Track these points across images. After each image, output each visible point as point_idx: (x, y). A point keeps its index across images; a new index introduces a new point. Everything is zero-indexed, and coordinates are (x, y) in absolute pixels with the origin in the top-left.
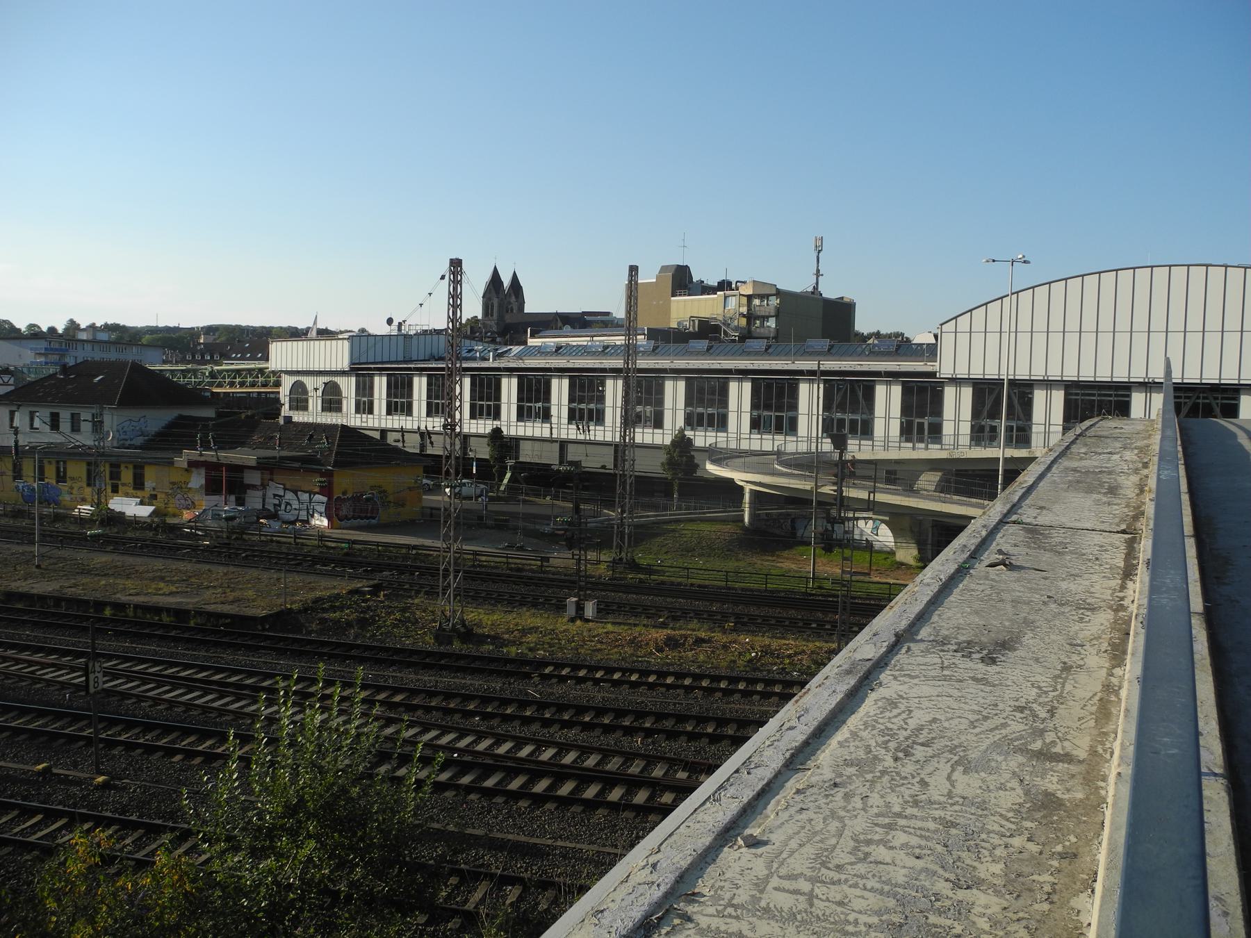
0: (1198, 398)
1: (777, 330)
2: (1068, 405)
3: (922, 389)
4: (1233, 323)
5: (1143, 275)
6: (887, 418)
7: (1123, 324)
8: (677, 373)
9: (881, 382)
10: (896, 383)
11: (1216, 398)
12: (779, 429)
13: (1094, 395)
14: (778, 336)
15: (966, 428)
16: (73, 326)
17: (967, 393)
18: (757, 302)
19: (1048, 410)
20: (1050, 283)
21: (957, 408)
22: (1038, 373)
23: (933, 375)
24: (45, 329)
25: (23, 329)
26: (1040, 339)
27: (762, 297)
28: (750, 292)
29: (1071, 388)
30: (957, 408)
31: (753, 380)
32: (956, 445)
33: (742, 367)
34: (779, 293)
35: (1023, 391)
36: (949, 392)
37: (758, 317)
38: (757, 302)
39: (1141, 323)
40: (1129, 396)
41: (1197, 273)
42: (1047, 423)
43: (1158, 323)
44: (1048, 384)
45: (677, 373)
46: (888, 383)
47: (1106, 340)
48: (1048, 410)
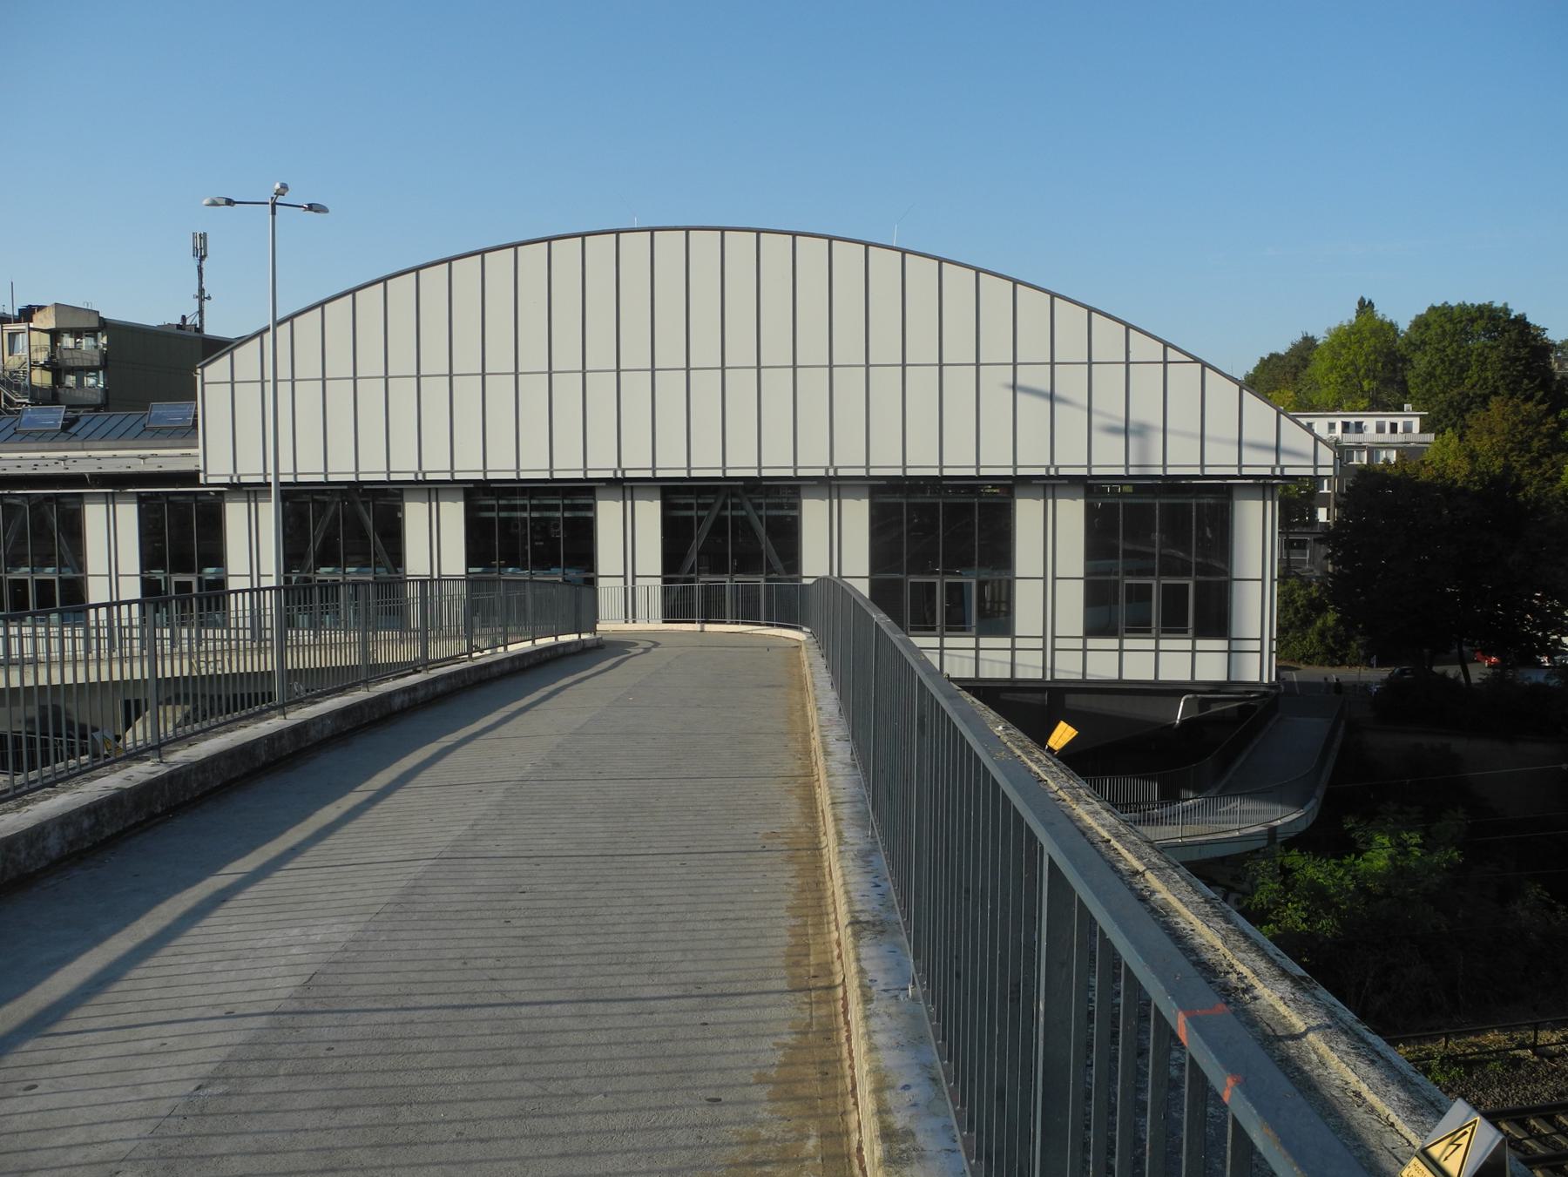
0: (724, 507)
1: (106, 391)
2: (675, 535)
3: (180, 508)
4: (284, 372)
5: (567, 252)
6: (1050, 579)
7: (602, 355)
8: (115, 484)
9: (95, 498)
10: (126, 498)
11: (758, 507)
12: (1173, 624)
13: (555, 508)
14: (106, 403)
15: (1072, 599)
16: (1506, 311)
17: (650, 513)
18: (68, 341)
19: (629, 542)
20: (384, 280)
21: (251, 547)
22: (602, 464)
23: (191, 478)
24: (1404, 325)
25: (1404, 325)
26: (742, 384)
27: (77, 333)
28: (51, 325)
29: (482, 497)
30: (251, 547)
31: (141, 500)
32: (1049, 641)
33: (110, 468)
34: (104, 325)
35: (577, 497)
36: (235, 514)
37: (72, 370)
38: (68, 341)
39: (403, 362)
40: (591, 507)
41: (705, 243)
42: (630, 575)
43: (705, 352)
44: (432, 489)
45: (115, 484)
46: (109, 500)
47: (500, 389)
48: (629, 542)
